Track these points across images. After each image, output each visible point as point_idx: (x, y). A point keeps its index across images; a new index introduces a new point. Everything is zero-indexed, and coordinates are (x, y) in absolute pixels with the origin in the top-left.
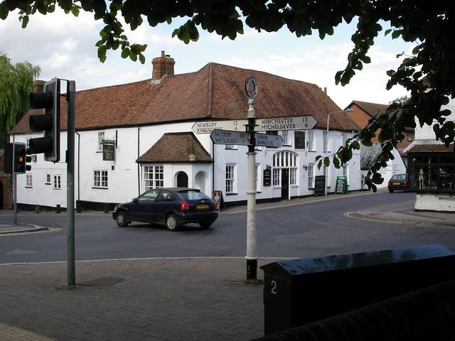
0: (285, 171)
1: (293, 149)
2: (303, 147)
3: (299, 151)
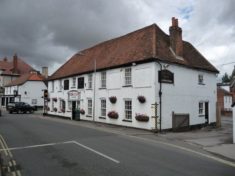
0: (74, 103)
1: (76, 89)
2: (83, 87)
3: (79, 90)
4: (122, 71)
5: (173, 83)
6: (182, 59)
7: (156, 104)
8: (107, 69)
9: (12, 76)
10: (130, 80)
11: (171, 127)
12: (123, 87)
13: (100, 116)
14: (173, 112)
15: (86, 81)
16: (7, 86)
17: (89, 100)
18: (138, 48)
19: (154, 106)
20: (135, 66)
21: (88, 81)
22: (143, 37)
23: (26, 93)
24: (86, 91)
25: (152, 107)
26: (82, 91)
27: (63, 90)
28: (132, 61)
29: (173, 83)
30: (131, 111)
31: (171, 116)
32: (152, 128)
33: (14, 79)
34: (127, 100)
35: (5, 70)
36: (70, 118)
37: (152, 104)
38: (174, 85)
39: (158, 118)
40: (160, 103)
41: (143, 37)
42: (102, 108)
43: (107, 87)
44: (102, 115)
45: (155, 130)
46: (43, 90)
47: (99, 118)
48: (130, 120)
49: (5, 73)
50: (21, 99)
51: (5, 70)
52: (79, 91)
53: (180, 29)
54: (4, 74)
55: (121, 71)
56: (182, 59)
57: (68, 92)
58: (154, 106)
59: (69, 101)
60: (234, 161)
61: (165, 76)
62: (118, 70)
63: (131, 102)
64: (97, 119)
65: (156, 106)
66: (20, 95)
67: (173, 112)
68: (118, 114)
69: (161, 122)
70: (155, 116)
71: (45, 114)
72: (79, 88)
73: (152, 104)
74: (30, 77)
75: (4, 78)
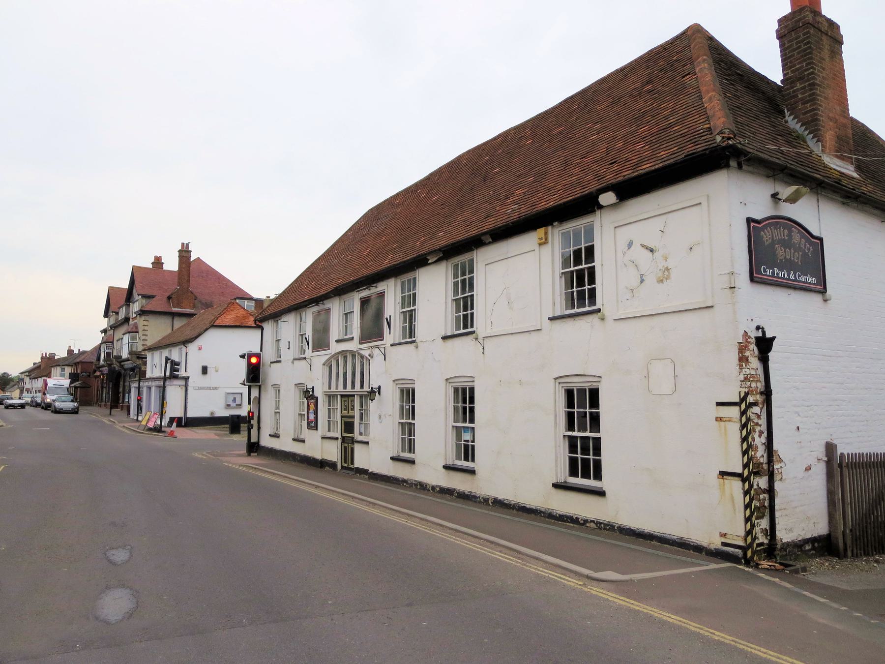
4: (546, 242)
5: (822, 289)
6: (849, 170)
7: (743, 403)
8: (475, 243)
9: (173, 315)
10: (587, 287)
11: (820, 528)
12: (551, 319)
13: (450, 463)
14: (830, 448)
15: (392, 308)
16: (153, 349)
17: (402, 391)
18: (623, 131)
19: (734, 412)
20: (613, 206)
21: (399, 309)
22: (643, 86)
23: (205, 370)
24: (392, 352)
25: (719, 419)
26: (376, 351)
27: (309, 353)
28: (593, 187)
29: (823, 291)
30: (597, 441)
31: (820, 471)
32: (724, 535)
33: (179, 323)
34: (576, 384)
35: (153, 297)
36: (333, 465)
37: (719, 404)
38: (825, 301)
39: (373, 406)
40: (767, 393)
41: (643, 86)
42: (575, 434)
43: (480, 325)
44: (458, 458)
45: (744, 549)
46: (242, 356)
47: (446, 467)
48: (591, 483)
49: (152, 305)
50: (189, 392)
51: (153, 297)
52: (366, 353)
53: (833, 26)
54: (147, 308)
55: (543, 243)
56: (849, 170)
57: (328, 357)
58: (734, 412)
59: (329, 396)
60: (345, 372)
61: (781, 253)
62: (528, 241)
63: (594, 394)
64: (437, 478)
65: (743, 413)
66: (186, 379)
67: (830, 448)
68: (606, 492)
69: (777, 501)
70: (739, 469)
71: (254, 448)
72: (364, 339)
73: (719, 404)
74: (221, 314)
75: (145, 323)
